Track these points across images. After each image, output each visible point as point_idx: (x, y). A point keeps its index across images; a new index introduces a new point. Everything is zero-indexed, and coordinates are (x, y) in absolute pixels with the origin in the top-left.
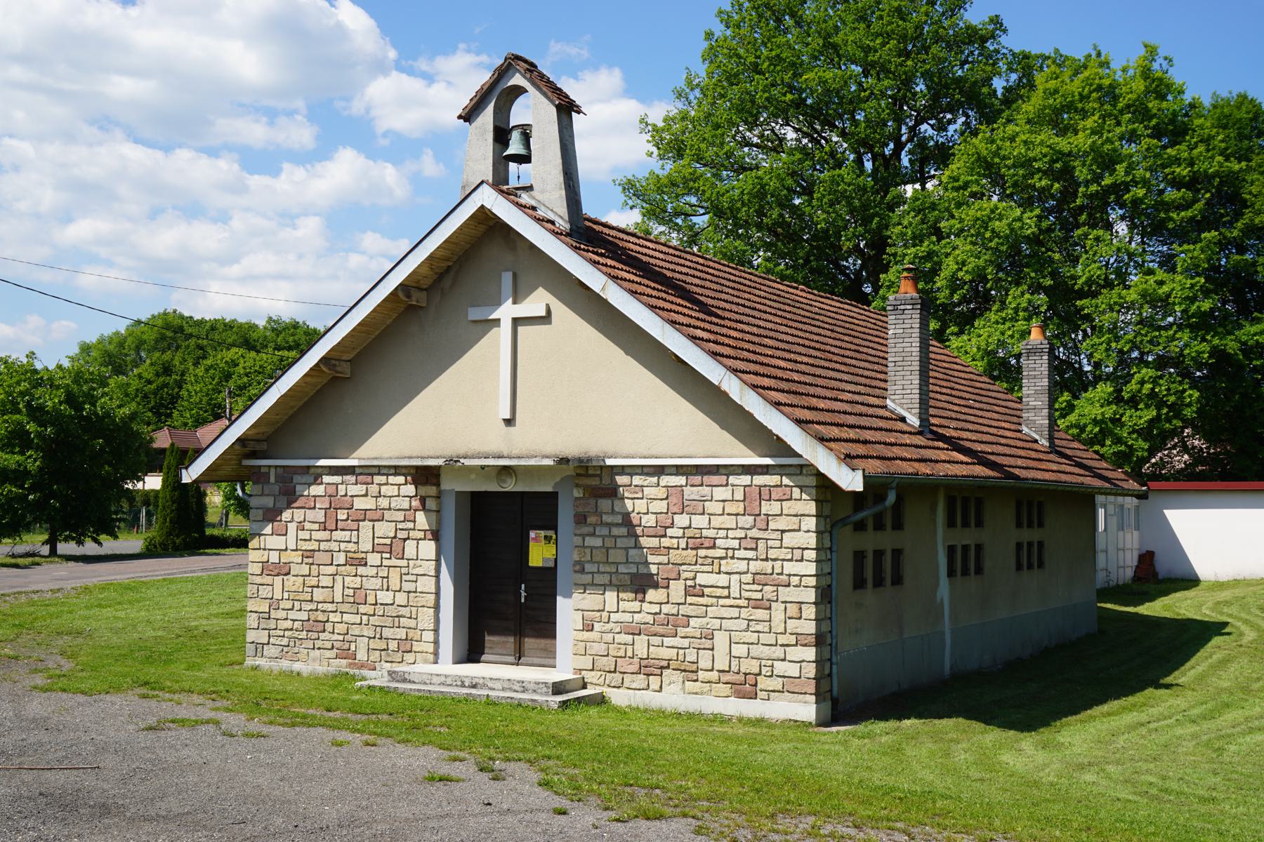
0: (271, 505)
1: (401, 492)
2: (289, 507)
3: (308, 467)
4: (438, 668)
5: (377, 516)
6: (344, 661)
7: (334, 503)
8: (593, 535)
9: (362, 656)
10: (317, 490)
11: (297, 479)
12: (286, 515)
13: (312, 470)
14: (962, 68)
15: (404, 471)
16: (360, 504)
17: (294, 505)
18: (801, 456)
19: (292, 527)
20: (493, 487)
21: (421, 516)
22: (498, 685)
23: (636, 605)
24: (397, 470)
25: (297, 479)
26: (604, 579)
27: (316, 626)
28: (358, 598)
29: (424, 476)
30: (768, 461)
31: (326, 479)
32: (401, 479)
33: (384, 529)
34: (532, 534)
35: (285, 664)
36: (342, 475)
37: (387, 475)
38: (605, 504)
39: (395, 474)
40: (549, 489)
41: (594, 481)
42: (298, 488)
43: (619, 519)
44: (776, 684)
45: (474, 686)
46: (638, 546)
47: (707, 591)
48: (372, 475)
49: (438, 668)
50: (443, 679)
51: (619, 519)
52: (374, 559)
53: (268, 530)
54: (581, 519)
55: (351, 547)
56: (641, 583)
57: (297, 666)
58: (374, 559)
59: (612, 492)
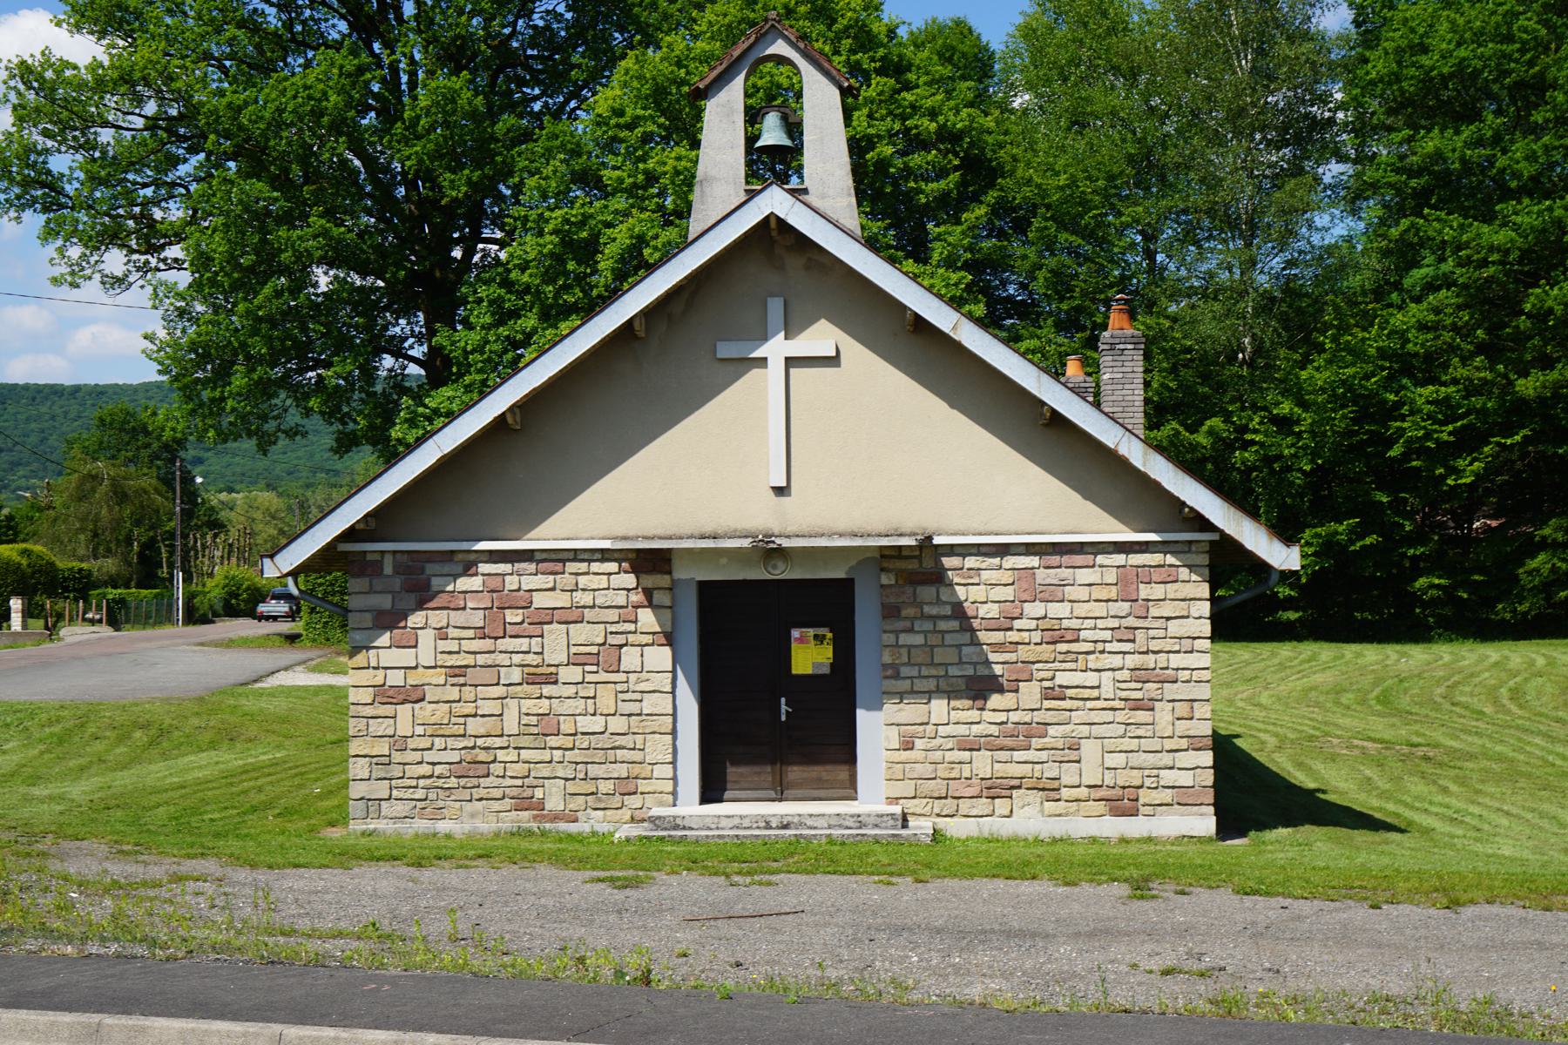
3: (452, 552)
4: (690, 807)
7: (500, 600)
8: (911, 630)
9: (554, 803)
11: (431, 568)
12: (416, 619)
13: (460, 557)
16: (540, 600)
23: (974, 715)
24: (604, 555)
25: (431, 568)
29: (649, 563)
31: (484, 568)
34: (795, 633)
35: (421, 825)
36: (512, 562)
39: (603, 560)
42: (435, 582)
47: (1069, 692)
56: (981, 687)
57: (443, 826)
58: (566, 674)
59: (938, 577)
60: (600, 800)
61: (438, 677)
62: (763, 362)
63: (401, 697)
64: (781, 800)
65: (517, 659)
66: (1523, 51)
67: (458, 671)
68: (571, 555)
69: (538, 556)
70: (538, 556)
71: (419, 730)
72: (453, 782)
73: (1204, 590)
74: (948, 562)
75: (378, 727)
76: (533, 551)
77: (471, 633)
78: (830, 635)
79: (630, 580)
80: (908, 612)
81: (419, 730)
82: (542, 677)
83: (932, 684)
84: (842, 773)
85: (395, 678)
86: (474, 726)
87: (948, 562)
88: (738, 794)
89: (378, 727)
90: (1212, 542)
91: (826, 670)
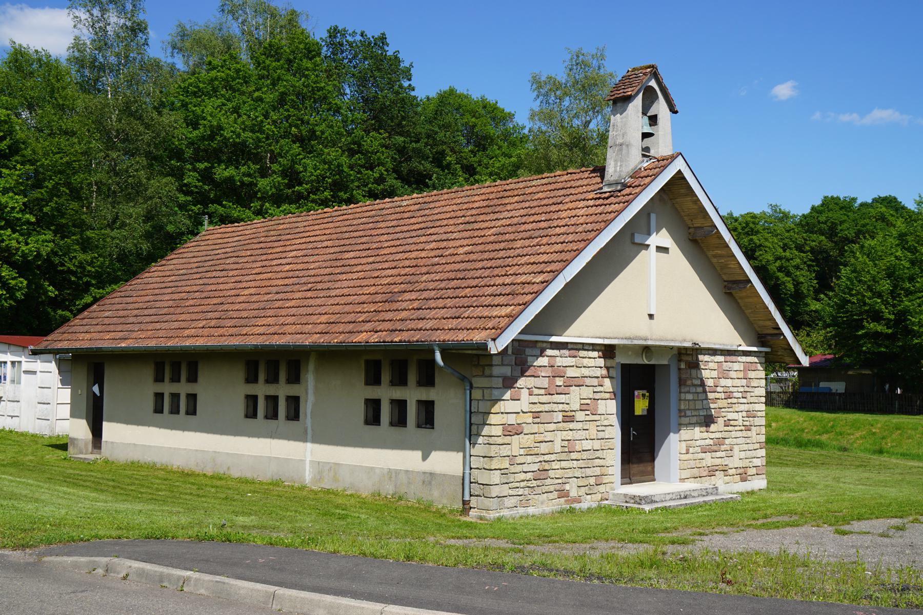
0: (509, 374)
1: (594, 363)
2: (522, 375)
3: (537, 342)
4: (618, 490)
5: (578, 382)
6: (563, 500)
7: (557, 373)
8: (689, 392)
9: (573, 493)
10: (542, 361)
11: (528, 351)
12: (521, 382)
13: (539, 345)
14: (208, 71)
15: (598, 348)
16: (571, 373)
17: (527, 374)
18: (507, 346)
19: (524, 393)
20: (639, 361)
21: (607, 382)
22: (695, 494)
23: (705, 435)
24: (593, 347)
25: (528, 351)
26: (694, 420)
27: (542, 474)
28: (569, 449)
29: (608, 351)
30: (755, 349)
31: (549, 352)
32: (595, 354)
33: (587, 392)
34: (636, 393)
35: (521, 511)
36: (559, 349)
37: (588, 350)
38: (694, 372)
39: (593, 350)
40: (666, 362)
41: (688, 357)
42: (530, 359)
43: (698, 382)
44: (754, 471)
45: (685, 497)
46: (707, 399)
47: (732, 423)
48: (579, 350)
49: (618, 490)
50: (671, 496)
51: (698, 382)
52: (580, 416)
53: (507, 395)
54: (682, 382)
55: (566, 407)
56: (708, 421)
57: (531, 510)
58: (580, 416)
59: (695, 365)
60: (590, 489)
61: (529, 418)
62: (648, 246)
63: (514, 431)
64: (631, 483)
65: (561, 407)
66: (267, 138)
67: (536, 414)
68: (581, 347)
69: (570, 346)
70: (570, 346)
71: (522, 452)
72: (534, 483)
73: (762, 374)
74: (701, 357)
75: (505, 450)
76: (567, 343)
77: (542, 392)
78: (647, 394)
79: (601, 362)
80: (689, 382)
81: (522, 452)
82: (569, 418)
83: (694, 420)
84: (650, 468)
85: (512, 419)
86: (544, 448)
87: (701, 357)
88: (638, 478)
89: (505, 450)
90: (766, 353)
91: (645, 413)
